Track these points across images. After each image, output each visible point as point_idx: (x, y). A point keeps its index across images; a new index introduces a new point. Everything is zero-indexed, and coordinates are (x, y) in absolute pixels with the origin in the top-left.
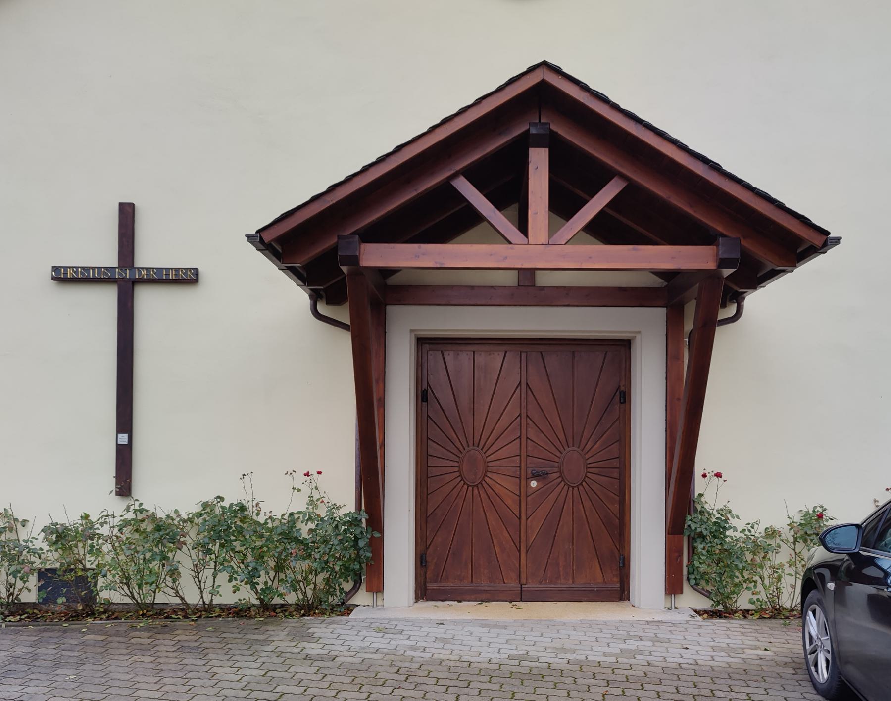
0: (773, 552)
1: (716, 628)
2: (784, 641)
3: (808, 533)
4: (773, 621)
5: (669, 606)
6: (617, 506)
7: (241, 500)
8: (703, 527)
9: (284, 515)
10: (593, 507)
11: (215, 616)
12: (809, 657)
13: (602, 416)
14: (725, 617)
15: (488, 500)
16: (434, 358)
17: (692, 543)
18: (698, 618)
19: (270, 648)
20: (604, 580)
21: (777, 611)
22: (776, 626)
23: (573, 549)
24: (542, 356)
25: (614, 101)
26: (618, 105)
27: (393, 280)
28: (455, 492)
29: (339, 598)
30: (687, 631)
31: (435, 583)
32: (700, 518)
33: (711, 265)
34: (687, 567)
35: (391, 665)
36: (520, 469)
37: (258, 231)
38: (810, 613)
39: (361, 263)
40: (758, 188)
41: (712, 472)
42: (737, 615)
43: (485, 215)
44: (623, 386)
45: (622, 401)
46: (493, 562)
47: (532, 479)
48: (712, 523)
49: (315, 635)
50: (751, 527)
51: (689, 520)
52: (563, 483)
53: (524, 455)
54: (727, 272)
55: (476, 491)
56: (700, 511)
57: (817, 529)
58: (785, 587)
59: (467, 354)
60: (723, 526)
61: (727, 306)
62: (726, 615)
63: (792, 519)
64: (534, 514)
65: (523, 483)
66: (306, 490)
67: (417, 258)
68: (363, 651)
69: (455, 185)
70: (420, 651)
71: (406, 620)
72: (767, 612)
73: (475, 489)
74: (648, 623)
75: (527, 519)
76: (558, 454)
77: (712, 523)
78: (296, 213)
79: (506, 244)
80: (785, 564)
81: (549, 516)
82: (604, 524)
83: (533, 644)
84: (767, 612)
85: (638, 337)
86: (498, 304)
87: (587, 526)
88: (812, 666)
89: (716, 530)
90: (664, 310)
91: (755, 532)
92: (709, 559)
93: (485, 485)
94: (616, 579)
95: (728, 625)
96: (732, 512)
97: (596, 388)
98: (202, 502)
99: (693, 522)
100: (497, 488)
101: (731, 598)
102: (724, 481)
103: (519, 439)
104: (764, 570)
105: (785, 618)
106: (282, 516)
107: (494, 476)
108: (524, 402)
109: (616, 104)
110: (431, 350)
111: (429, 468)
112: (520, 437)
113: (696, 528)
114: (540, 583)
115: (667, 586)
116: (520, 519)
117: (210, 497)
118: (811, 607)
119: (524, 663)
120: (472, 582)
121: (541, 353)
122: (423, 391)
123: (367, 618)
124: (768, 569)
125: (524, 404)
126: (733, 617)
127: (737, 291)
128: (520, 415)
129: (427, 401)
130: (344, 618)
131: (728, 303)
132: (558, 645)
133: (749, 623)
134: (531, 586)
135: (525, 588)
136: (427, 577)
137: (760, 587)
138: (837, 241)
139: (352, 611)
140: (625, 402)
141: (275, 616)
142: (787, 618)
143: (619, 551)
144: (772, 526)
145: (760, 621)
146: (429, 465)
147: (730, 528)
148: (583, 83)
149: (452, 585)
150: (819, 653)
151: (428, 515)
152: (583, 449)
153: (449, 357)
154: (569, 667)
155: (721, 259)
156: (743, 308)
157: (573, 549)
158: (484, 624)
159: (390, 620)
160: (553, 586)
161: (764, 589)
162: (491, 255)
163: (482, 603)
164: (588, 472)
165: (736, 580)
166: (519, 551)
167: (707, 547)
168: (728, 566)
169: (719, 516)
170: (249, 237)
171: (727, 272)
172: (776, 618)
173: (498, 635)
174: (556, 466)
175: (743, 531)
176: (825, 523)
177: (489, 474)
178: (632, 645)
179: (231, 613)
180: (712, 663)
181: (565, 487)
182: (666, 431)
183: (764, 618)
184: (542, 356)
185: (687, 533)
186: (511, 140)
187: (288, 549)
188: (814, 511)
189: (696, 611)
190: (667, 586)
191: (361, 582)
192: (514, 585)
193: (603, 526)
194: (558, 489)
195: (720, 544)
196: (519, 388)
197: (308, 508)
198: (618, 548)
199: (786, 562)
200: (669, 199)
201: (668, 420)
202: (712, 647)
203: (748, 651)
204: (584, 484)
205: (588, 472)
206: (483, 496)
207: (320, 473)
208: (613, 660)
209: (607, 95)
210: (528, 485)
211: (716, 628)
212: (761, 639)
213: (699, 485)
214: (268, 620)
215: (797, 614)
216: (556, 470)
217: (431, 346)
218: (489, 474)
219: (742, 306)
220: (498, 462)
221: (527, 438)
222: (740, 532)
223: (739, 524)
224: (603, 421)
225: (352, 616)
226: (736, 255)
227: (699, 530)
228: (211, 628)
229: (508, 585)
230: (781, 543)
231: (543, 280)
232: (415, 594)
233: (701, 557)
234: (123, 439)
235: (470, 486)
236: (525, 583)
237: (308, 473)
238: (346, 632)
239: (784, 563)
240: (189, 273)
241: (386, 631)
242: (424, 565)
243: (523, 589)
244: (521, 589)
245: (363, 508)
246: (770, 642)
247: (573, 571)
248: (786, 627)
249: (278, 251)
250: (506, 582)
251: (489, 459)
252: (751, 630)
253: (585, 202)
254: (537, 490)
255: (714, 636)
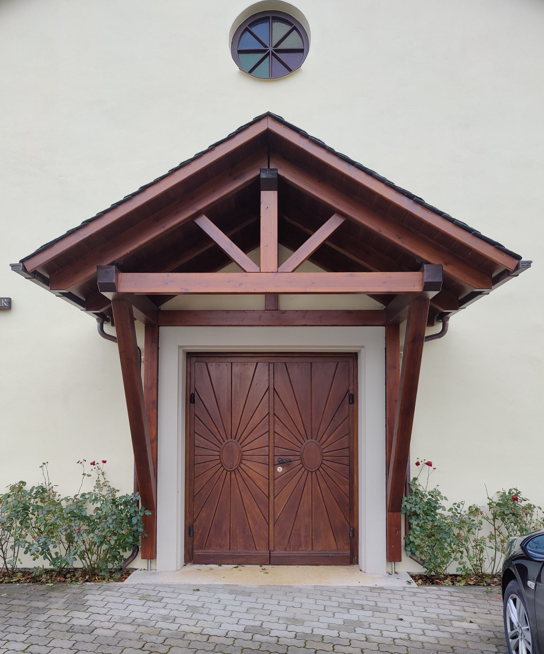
0: (476, 529)
1: (428, 596)
2: (487, 612)
3: (506, 513)
4: (477, 588)
5: (390, 571)
6: (347, 487)
7: (42, 484)
8: (417, 506)
9: (76, 495)
10: (328, 488)
11: (15, 581)
12: (510, 640)
13: (335, 414)
14: (437, 583)
15: (243, 482)
16: (199, 367)
17: (408, 520)
18: (414, 584)
19: (43, 617)
20: (337, 547)
21: (480, 577)
22: (479, 593)
23: (312, 522)
24: (286, 366)
25: (329, 146)
26: (333, 149)
27: (167, 306)
28: (217, 476)
29: (118, 565)
30: (403, 599)
31: (201, 549)
32: (414, 499)
33: (418, 288)
34: (404, 539)
35: (140, 639)
36: (269, 458)
37: (22, 261)
38: (511, 601)
39: (118, 289)
40: (457, 219)
41: (425, 460)
42: (446, 581)
43: (223, 248)
44: (352, 390)
45: (351, 402)
46: (247, 533)
47: (279, 465)
48: (425, 503)
49: (88, 603)
50: (457, 506)
51: (405, 501)
52: (303, 469)
53: (271, 445)
54: (432, 294)
55: (233, 475)
56: (415, 493)
57: (513, 510)
58: (487, 558)
59: (226, 365)
60: (433, 506)
61: (435, 324)
62: (437, 581)
63: (491, 500)
64: (280, 493)
65: (271, 469)
66: (94, 475)
67: (165, 285)
68: (121, 621)
69: (198, 223)
70: (170, 621)
71: (169, 586)
72: (472, 579)
73: (233, 473)
74: (372, 589)
75: (274, 498)
76: (299, 445)
77: (425, 503)
78: (54, 245)
79: (241, 272)
80: (486, 538)
81: (292, 495)
82: (336, 501)
83: (269, 613)
84: (472, 579)
85: (363, 351)
86: (249, 324)
87: (323, 504)
88: (514, 650)
89: (428, 509)
90: (383, 328)
91: (461, 511)
92: (422, 533)
93: (241, 470)
94: (347, 547)
95: (439, 593)
96: (441, 495)
97: (330, 391)
98: (11, 485)
99: (409, 502)
100: (251, 473)
101: (441, 567)
102: (434, 469)
103: (268, 433)
104: (468, 544)
105: (487, 586)
106: (74, 497)
107: (248, 463)
108: (272, 403)
109: (331, 148)
110: (197, 362)
111: (195, 457)
113: (411, 508)
114: (285, 550)
115: (388, 555)
116: (269, 497)
117: (15, 481)
118: (511, 595)
119: (257, 637)
120: (230, 549)
121: (285, 363)
122: (191, 395)
123: (138, 584)
124: (472, 542)
125: (272, 405)
126: (443, 583)
127: (442, 312)
128: (269, 413)
129: (194, 402)
130: (120, 583)
131: (435, 322)
132: (291, 616)
133: (456, 591)
134: (278, 552)
135: (274, 554)
136: (194, 545)
137: (465, 559)
138: (528, 264)
139: (130, 574)
140: (353, 402)
141: (64, 582)
142: (489, 585)
143: (349, 524)
144: (474, 504)
145: (466, 587)
146: (195, 454)
147: (440, 507)
148: (302, 130)
149: (214, 551)
150: (520, 641)
151: (195, 495)
152: (320, 441)
153: (212, 367)
154: (295, 642)
155: (425, 283)
156: (447, 326)
157: (312, 522)
158: (234, 591)
159: (156, 585)
160: (296, 552)
161: (469, 561)
162: (228, 282)
163: (237, 567)
164: (324, 460)
165: (446, 551)
166: (268, 524)
167: (421, 523)
168: (438, 540)
169: (430, 497)
170: (14, 267)
171: (432, 294)
172: (480, 585)
173: (241, 603)
174: (298, 455)
175: (451, 509)
176: (519, 503)
177: (244, 462)
178: (354, 615)
179: (29, 578)
180: (422, 638)
181: (305, 472)
182: (386, 427)
183: (470, 584)
184: (286, 366)
185: (403, 511)
186: (244, 184)
187: (73, 526)
188: (509, 493)
189: (412, 576)
190: (388, 555)
191: (138, 550)
192: (264, 551)
193: (336, 503)
194: (300, 473)
195: (431, 521)
196: (268, 392)
197: (94, 491)
198: (349, 522)
199: (487, 536)
200: (380, 232)
201: (387, 418)
202: (424, 619)
203: (456, 624)
204: (320, 469)
205: (324, 460)
206: (239, 479)
207: (104, 462)
208: (334, 633)
209: (323, 141)
210: (275, 470)
211: (428, 596)
212: (467, 609)
213: (413, 471)
214: (57, 585)
215: (497, 581)
216: (298, 458)
217: (198, 359)
218: (244, 462)
219: (447, 324)
220: (251, 452)
221: (274, 432)
222: (448, 511)
223: (447, 504)
224: (336, 418)
225: (127, 582)
226: (439, 279)
227: (413, 509)
228: (6, 594)
229: (260, 552)
230: (483, 520)
231: (286, 303)
232: (184, 559)
233: (416, 532)
235: (229, 471)
236: (273, 550)
237: (94, 462)
238: (115, 599)
239: (486, 536)
240: (3, 302)
241: (148, 599)
242: (191, 535)
243: (271, 555)
244: (270, 555)
246: (475, 613)
247: (312, 540)
248: (489, 595)
249: (46, 278)
250: (257, 549)
251: (244, 449)
252: (458, 598)
253: (308, 236)
254: (282, 474)
255: (426, 605)
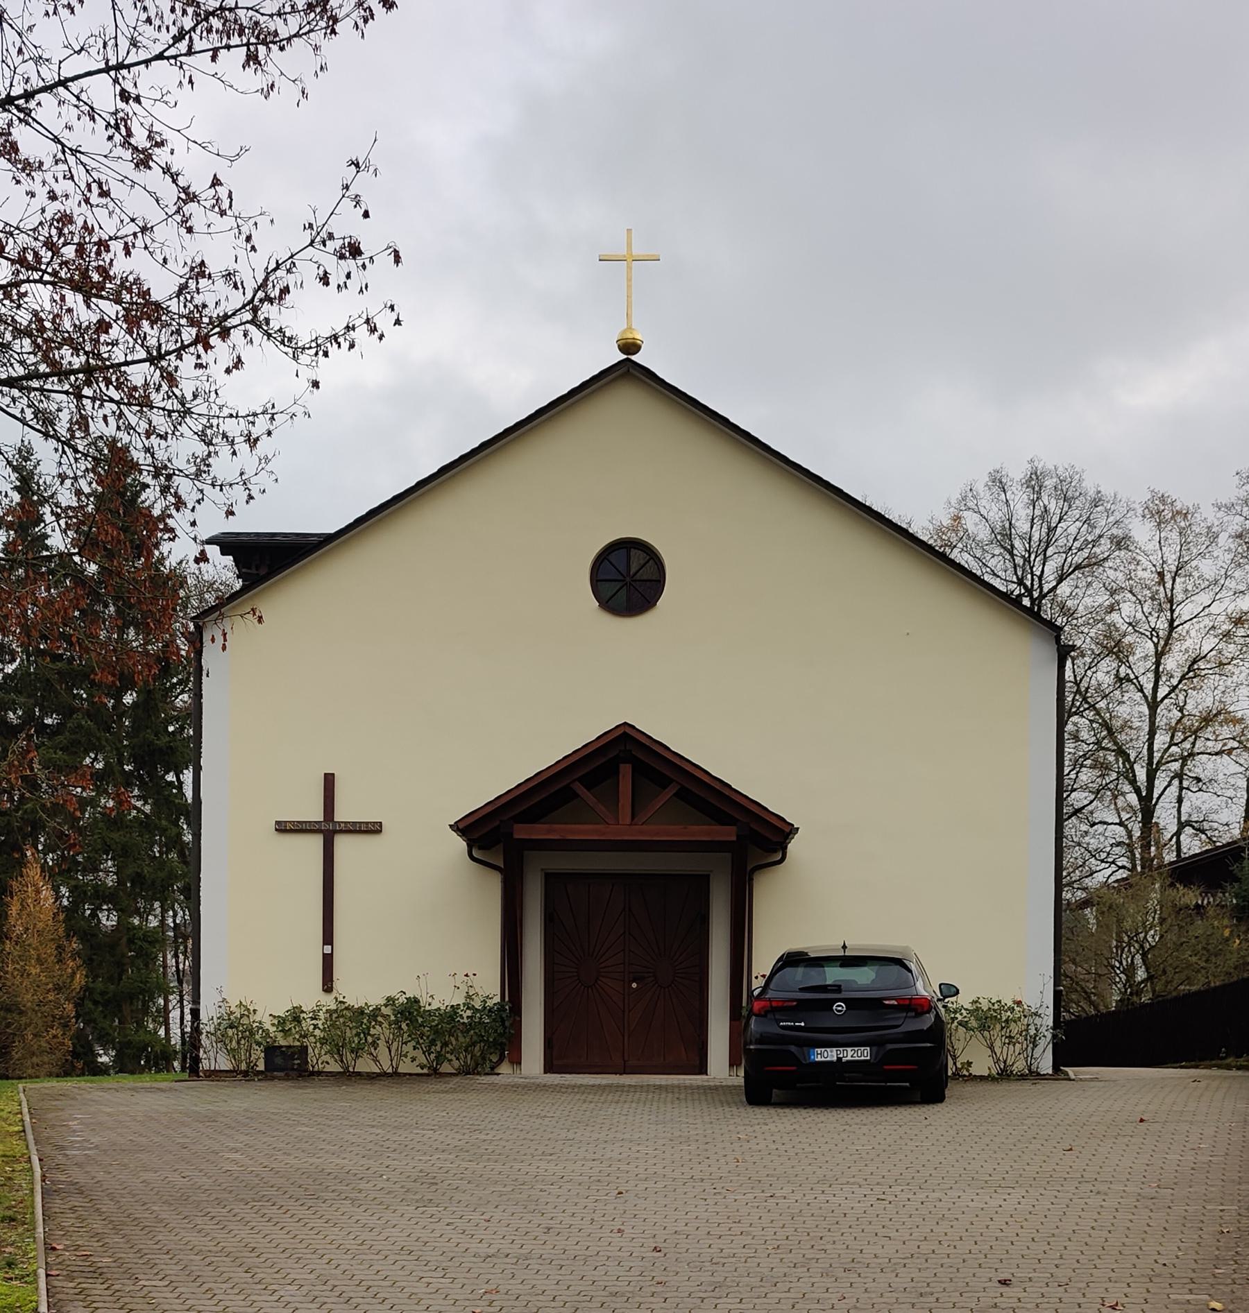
66: (464, 988)
112: (624, 950)
116: (624, 1011)
138: (798, 829)
170: (451, 826)
234: (328, 949)
245: (507, 999)
